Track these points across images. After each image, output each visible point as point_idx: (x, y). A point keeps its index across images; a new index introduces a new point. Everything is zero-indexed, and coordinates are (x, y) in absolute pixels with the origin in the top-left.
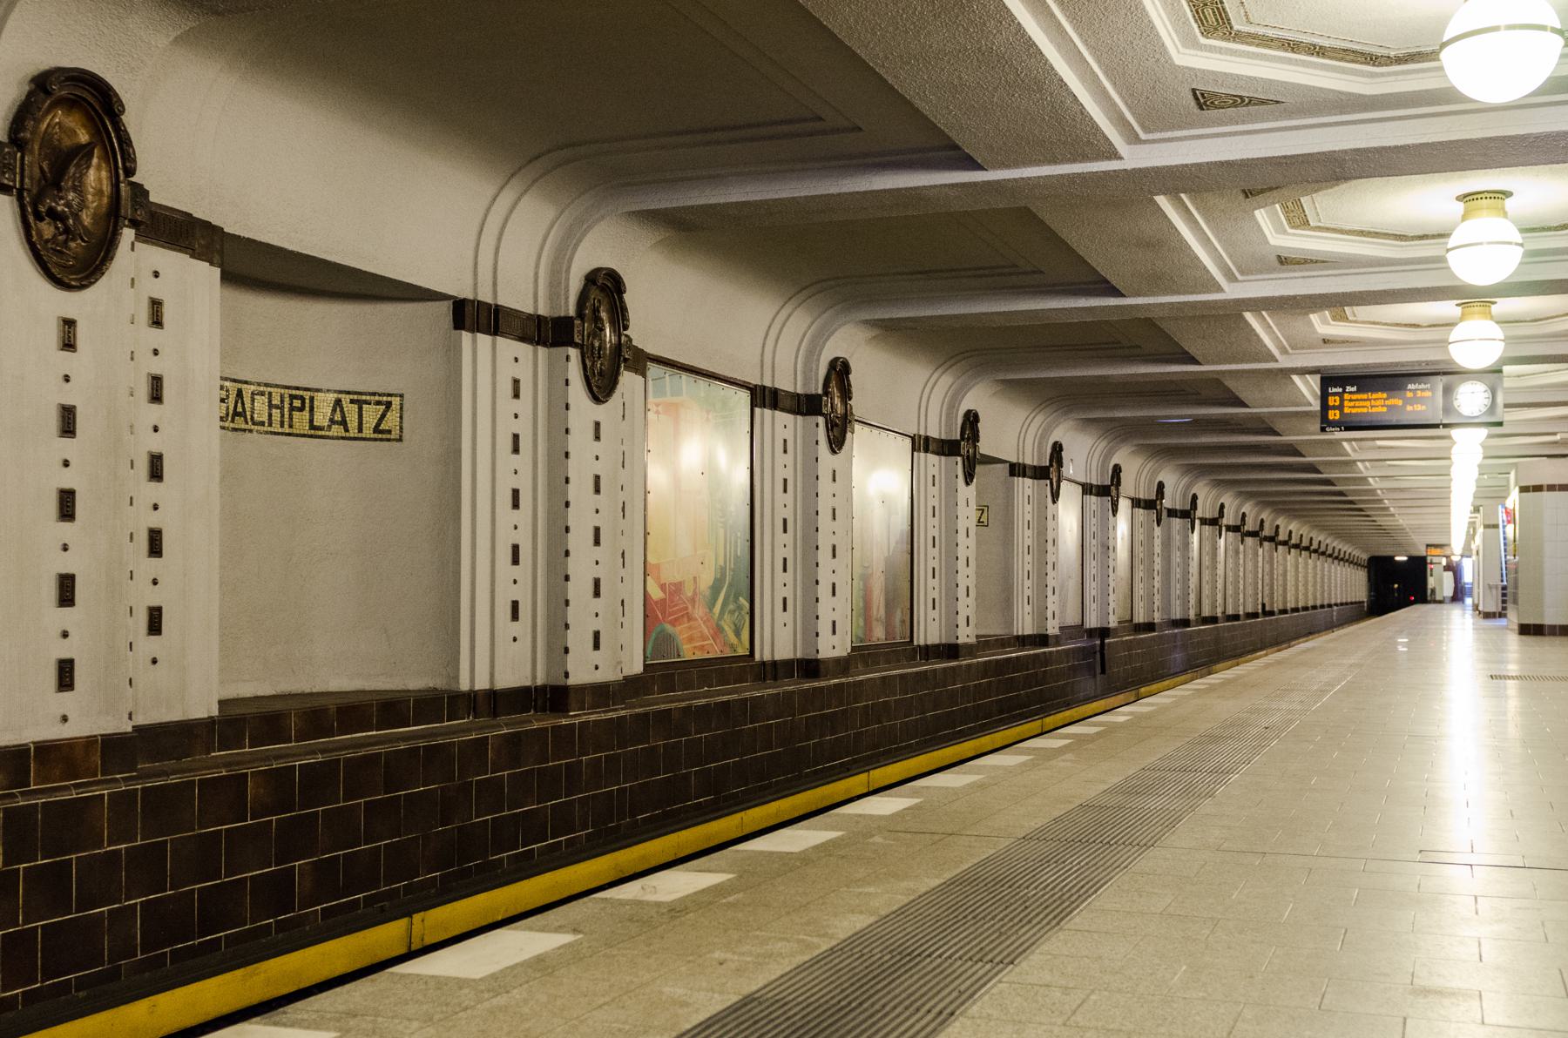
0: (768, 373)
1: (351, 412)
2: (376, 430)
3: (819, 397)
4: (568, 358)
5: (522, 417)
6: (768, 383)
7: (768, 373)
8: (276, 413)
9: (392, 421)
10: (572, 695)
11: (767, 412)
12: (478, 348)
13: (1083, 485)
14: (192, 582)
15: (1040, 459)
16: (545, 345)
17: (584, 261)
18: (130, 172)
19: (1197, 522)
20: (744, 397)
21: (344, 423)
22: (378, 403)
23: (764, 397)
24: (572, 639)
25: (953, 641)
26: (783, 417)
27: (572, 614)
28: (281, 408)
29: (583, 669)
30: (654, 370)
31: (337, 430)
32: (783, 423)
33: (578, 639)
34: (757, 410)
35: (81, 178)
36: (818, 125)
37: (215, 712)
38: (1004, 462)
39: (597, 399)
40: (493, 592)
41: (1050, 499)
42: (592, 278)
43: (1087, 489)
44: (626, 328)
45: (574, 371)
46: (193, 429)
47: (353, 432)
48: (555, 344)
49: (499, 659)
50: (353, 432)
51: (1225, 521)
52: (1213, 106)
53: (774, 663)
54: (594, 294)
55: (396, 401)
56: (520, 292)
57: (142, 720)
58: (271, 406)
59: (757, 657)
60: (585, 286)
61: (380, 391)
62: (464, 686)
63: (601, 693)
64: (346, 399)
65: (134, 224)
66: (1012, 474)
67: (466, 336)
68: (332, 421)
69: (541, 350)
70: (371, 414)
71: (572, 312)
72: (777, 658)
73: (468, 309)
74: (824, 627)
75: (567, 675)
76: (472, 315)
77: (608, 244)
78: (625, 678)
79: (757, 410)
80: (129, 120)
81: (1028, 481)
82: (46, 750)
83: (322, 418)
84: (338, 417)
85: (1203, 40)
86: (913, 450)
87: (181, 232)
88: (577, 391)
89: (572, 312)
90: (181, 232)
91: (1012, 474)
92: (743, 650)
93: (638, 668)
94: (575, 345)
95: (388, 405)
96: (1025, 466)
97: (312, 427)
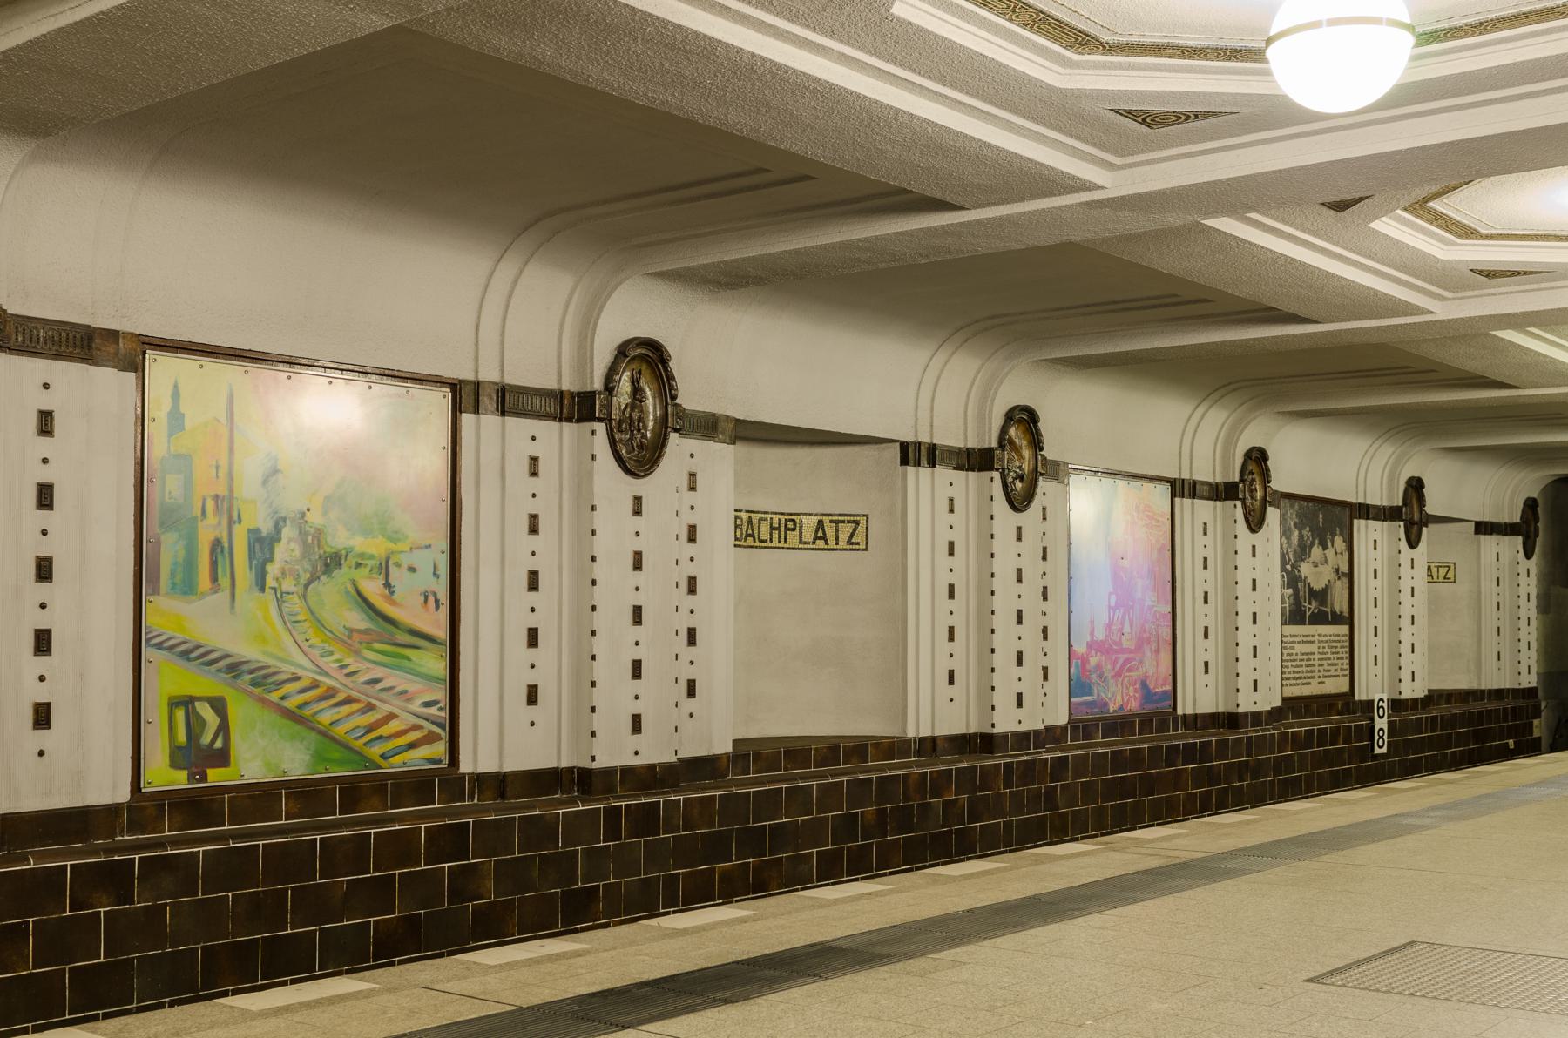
0: (1185, 463)
1: (1434, 570)
2: (849, 542)
3: (990, 451)
4: (593, 433)
5: (963, 528)
6: (1186, 476)
7: (1185, 463)
8: (775, 533)
9: (1450, 575)
11: (1187, 501)
12: (921, 478)
13: (1172, 482)
14: (717, 661)
15: (1390, 497)
16: (569, 420)
17: (613, 329)
18: (674, 397)
23: (1482, 528)
24: (997, 698)
25: (1232, 709)
26: (944, 474)
27: (997, 679)
28: (778, 529)
29: (1248, 703)
30: (161, 367)
31: (821, 544)
32: (1205, 510)
33: (1244, 683)
37: (729, 749)
39: (1253, 531)
42: (1248, 455)
45: (1239, 513)
46: (719, 557)
49: (936, 712)
50: (832, 544)
53: (934, 739)
54: (1252, 467)
55: (863, 520)
56: (1205, 471)
57: (684, 754)
58: (772, 528)
59: (1180, 712)
60: (616, 357)
62: (911, 734)
63: (1256, 718)
64: (826, 520)
65: (676, 430)
66: (905, 461)
67: (910, 469)
68: (816, 538)
70: (1443, 571)
71: (994, 444)
72: (1200, 711)
73: (911, 450)
74: (1405, 675)
75: (593, 759)
76: (911, 454)
77: (637, 309)
78: (1047, 729)
80: (673, 365)
82: (627, 772)
83: (808, 536)
84: (820, 534)
86: (1173, 496)
87: (708, 426)
88: (1000, 505)
89: (994, 444)
90: (708, 426)
91: (905, 461)
92: (1345, 688)
93: (1278, 703)
94: (600, 420)
95: (857, 523)
97: (801, 541)
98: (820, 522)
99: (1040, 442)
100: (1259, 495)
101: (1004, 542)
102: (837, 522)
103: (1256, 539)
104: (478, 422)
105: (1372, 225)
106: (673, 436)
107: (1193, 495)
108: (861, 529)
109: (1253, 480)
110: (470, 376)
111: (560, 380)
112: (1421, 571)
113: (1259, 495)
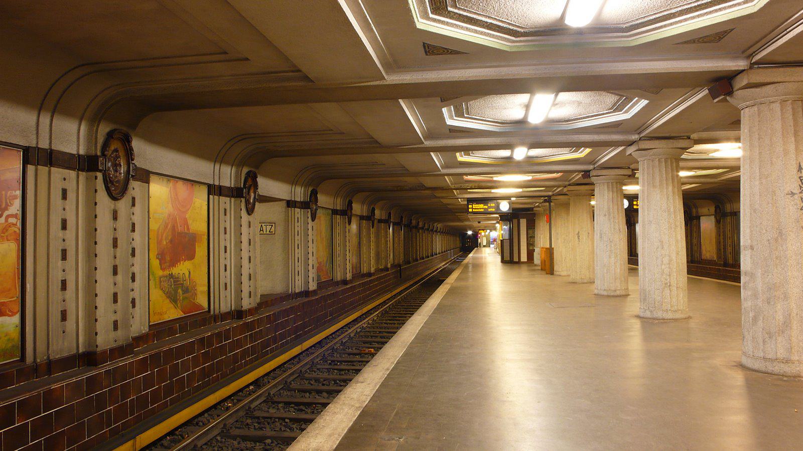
3: (97, 157)
4: (96, 178)
7: (293, 196)
10: (739, 131)
16: (83, 171)
19: (376, 222)
20: (204, 191)
21: (263, 230)
22: (270, 225)
34: (211, 196)
35: (621, 271)
36: (331, 132)
38: (330, 209)
39: (249, 214)
40: (219, 274)
41: (371, 227)
43: (362, 218)
44: (133, 160)
47: (265, 233)
48: (88, 171)
51: (425, 228)
52: (433, 54)
61: (266, 222)
64: (263, 225)
69: (233, 199)
79: (211, 196)
81: (298, 210)
85: (431, 16)
86: (360, 220)
88: (102, 196)
94: (101, 171)
95: (272, 226)
96: (295, 202)
98: (262, 225)
99: (132, 154)
100: (123, 170)
101: (104, 221)
102: (266, 226)
103: (251, 218)
104: (219, 198)
105: (400, 101)
106: (257, 204)
107: (220, 194)
108: (273, 228)
109: (118, 157)
110: (212, 183)
111: (231, 184)
112: (256, 227)
113: (123, 170)
